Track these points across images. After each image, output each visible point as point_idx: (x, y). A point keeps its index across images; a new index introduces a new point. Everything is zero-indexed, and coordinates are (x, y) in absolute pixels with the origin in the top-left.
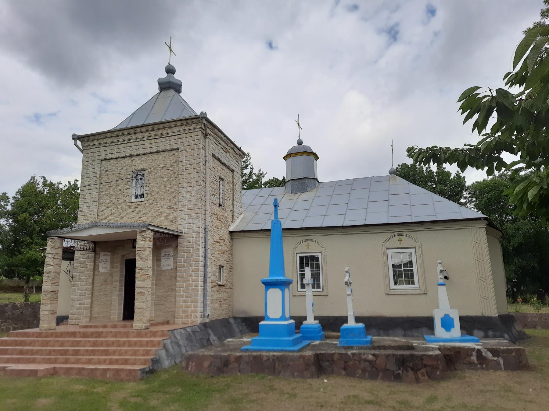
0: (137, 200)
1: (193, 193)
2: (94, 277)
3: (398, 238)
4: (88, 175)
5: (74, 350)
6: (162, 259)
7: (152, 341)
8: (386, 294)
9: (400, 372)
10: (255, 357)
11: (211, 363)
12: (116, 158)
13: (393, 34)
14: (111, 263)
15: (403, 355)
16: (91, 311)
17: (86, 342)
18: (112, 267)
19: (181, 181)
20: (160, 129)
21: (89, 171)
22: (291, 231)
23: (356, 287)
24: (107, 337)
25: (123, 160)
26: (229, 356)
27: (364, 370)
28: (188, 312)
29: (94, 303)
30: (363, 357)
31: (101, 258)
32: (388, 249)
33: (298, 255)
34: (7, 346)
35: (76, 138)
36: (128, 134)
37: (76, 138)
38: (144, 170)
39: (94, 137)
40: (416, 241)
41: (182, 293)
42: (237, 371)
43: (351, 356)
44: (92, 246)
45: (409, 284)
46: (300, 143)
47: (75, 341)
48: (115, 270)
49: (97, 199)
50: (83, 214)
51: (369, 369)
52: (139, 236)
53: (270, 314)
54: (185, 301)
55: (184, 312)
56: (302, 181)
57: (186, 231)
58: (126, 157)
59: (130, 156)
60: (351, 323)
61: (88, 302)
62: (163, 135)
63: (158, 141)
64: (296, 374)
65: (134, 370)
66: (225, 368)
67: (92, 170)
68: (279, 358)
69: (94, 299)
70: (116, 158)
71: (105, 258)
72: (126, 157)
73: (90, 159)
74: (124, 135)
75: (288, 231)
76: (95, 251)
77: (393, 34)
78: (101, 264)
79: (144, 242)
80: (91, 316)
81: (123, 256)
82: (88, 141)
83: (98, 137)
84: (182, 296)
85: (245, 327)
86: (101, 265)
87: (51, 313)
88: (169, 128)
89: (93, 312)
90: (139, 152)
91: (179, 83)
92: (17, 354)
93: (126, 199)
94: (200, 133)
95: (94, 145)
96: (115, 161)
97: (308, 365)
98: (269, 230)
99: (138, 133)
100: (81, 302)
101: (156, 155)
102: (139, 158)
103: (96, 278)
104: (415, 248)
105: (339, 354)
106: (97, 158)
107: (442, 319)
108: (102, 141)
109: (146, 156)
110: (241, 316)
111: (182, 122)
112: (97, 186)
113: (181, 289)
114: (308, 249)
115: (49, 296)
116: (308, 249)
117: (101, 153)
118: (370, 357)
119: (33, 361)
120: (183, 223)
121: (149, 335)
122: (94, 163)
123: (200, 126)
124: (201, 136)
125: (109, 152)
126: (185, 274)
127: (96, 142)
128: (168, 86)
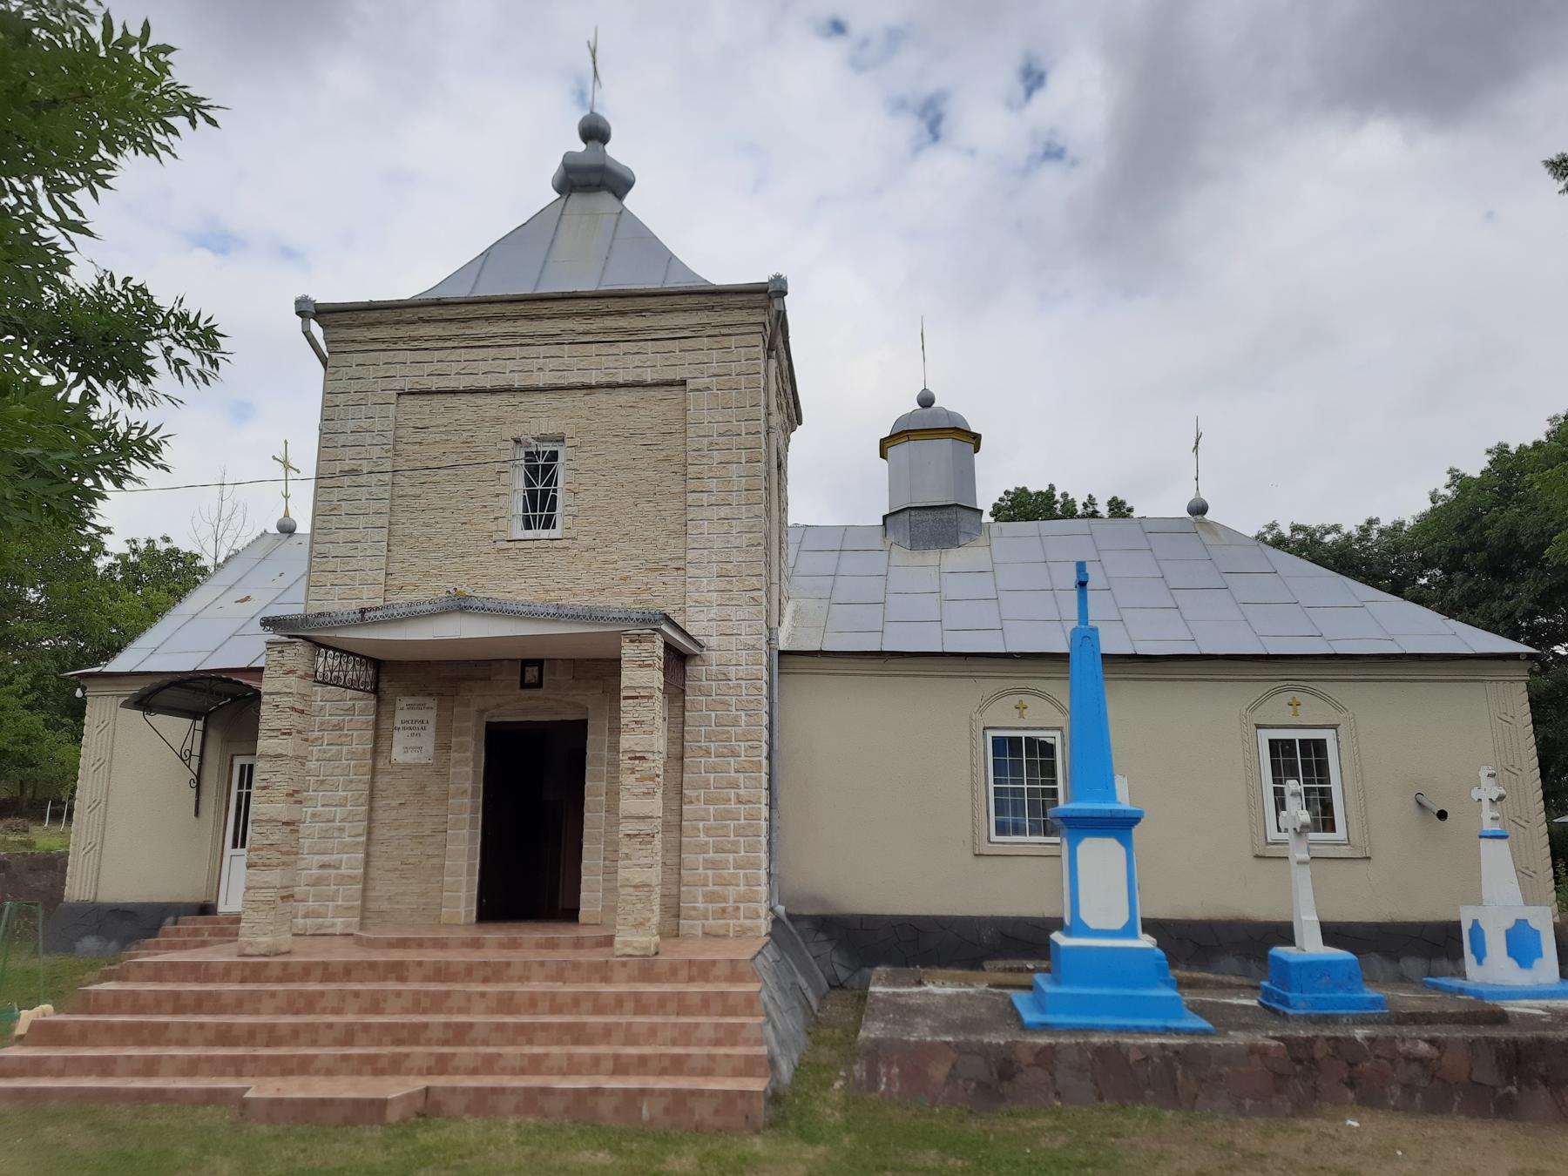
0: (530, 534)
1: (737, 526)
3: (1287, 697)
4: (351, 437)
5: (447, 1025)
8: (1257, 857)
9: (1514, 1090)
10: (1100, 1051)
11: (954, 1066)
12: (454, 392)
13: (932, 120)
14: (438, 730)
15: (1515, 1042)
16: (365, 890)
17: (342, 995)
18: (443, 747)
19: (692, 484)
20: (622, 313)
21: (351, 425)
22: (970, 661)
23: (1182, 827)
24: (528, 979)
25: (480, 400)
26: (1010, 1046)
27: (1409, 1088)
28: (725, 900)
30: (1402, 1048)
31: (400, 716)
32: (1258, 727)
33: (990, 734)
34: (101, 1012)
35: (308, 310)
36: (595, 314)
37: (308, 310)
38: (560, 439)
39: (376, 315)
40: (1339, 708)
41: (703, 838)
42: (1051, 1095)
43: (1366, 1044)
44: (367, 674)
45: (1325, 830)
46: (926, 401)
47: (427, 993)
48: (454, 755)
49: (384, 520)
50: (331, 567)
51: (1424, 1083)
52: (628, 650)
53: (1091, 916)
54: (713, 865)
55: (711, 897)
56: (945, 515)
57: (713, 642)
58: (493, 391)
60: (1310, 945)
61: (351, 862)
64: (1248, 1103)
65: (742, 1093)
66: (1006, 1084)
67: (365, 424)
68: (1177, 1051)
69: (375, 849)
70: (454, 392)
71: (416, 715)
72: (493, 391)
73: (356, 385)
74: (487, 319)
75: (961, 661)
76: (376, 691)
77: (932, 120)
78: (397, 736)
79: (646, 672)
80: (364, 909)
81: (481, 712)
82: (349, 327)
84: (703, 848)
85: (828, 948)
86: (400, 738)
87: (283, 898)
88: (655, 312)
89: (370, 894)
90: (542, 380)
92: (210, 1043)
94: (758, 339)
95: (374, 340)
96: (449, 401)
97: (1279, 1076)
98: (1063, 658)
99: (540, 318)
100: (326, 859)
101: (601, 397)
102: (542, 398)
103: (382, 781)
104: (1335, 727)
105: (1328, 1039)
106: (382, 384)
107: (1507, 932)
108: (404, 331)
109: (568, 399)
110: (806, 912)
111: (702, 299)
112: (387, 478)
113: (701, 825)
114: (1021, 716)
116: (1021, 716)
117: (397, 370)
118: (1423, 1047)
119: (303, 1067)
120: (702, 616)
121: (683, 974)
122: (371, 399)
123: (760, 319)
124: (760, 351)
125: (428, 368)
128: (595, 178)
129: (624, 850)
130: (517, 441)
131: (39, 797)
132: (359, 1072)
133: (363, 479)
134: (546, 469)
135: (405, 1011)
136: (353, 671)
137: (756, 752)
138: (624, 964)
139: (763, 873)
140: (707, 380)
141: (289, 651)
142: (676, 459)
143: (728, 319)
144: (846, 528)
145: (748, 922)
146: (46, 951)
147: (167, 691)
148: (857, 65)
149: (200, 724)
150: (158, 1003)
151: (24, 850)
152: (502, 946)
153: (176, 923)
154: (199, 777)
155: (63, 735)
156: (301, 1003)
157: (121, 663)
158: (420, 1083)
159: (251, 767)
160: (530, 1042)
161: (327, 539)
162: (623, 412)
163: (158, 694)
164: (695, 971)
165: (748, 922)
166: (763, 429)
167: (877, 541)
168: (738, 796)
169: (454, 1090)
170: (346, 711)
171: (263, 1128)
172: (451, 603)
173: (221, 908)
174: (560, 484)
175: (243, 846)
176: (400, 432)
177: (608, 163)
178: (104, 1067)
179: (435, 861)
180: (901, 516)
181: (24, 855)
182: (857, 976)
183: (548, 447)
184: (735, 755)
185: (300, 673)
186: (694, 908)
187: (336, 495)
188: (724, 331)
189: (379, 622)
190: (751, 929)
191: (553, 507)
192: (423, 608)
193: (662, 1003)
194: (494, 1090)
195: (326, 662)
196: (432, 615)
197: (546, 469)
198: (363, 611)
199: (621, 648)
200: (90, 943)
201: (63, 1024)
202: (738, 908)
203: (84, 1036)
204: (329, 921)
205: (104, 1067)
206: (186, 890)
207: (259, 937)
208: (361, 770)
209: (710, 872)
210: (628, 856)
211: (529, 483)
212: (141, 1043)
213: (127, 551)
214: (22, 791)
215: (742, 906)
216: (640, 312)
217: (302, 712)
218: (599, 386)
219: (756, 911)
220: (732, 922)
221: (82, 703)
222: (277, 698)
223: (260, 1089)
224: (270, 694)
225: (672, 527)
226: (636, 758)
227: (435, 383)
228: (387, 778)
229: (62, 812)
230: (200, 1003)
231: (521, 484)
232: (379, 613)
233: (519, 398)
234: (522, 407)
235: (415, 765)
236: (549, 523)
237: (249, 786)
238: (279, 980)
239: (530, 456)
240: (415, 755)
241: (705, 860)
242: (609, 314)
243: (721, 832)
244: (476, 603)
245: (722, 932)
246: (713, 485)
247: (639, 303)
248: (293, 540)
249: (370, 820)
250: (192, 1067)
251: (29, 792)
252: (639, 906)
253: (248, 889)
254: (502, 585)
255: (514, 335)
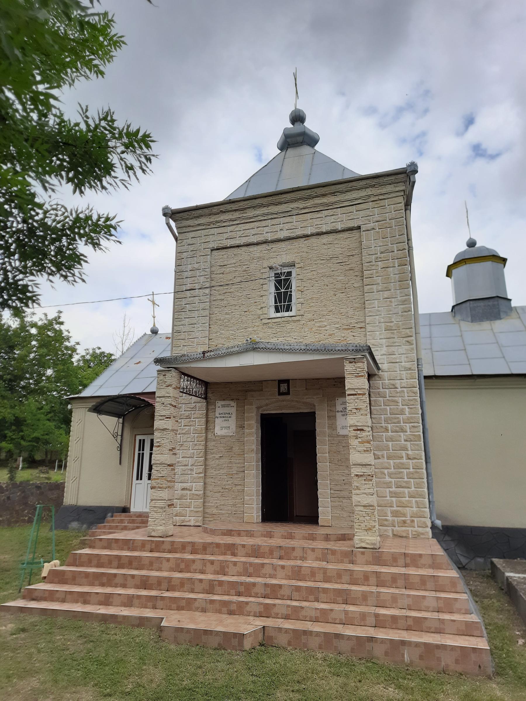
2: (206, 442)
6: (339, 415)
7: (406, 576)
16: (204, 502)
20: (324, 195)
21: (190, 267)
24: (306, 559)
28: (404, 515)
29: (210, 488)
31: (218, 411)
36: (262, 206)
39: (200, 212)
41: (388, 479)
46: (471, 244)
48: (246, 431)
49: (207, 313)
52: (348, 367)
55: (395, 514)
56: (491, 303)
58: (257, 244)
59: (266, 242)
62: (327, 205)
63: (319, 215)
67: (196, 266)
70: (238, 246)
71: (226, 410)
72: (257, 244)
73: (191, 248)
76: (206, 398)
80: (204, 512)
81: (258, 408)
82: (187, 219)
83: (206, 211)
87: (169, 505)
88: (342, 192)
89: (207, 504)
90: (282, 235)
91: (316, 137)
93: (260, 312)
94: (401, 199)
95: (199, 225)
96: (236, 251)
99: (280, 203)
100: (185, 485)
101: (313, 240)
102: (283, 245)
103: (211, 444)
108: (213, 219)
111: (368, 181)
112: (207, 291)
113: (386, 471)
115: (163, 473)
125: (226, 236)
126: (390, 444)
127: (202, 221)
128: (300, 139)
129: (355, 484)
130: (271, 268)
131: (53, 459)
132: (220, 612)
133: (197, 292)
134: (286, 280)
135: (239, 574)
136: (194, 386)
137: (416, 429)
138: (363, 553)
139: (427, 500)
140: (372, 224)
141: (168, 375)
142: (357, 269)
143: (384, 191)
144: (430, 314)
145: (420, 530)
146: (56, 528)
147: (107, 404)
148: (382, 126)
149: (121, 420)
150: (110, 562)
151: (46, 481)
152: (284, 537)
153: (112, 516)
154: (121, 445)
155: (62, 431)
156: (183, 566)
157: (87, 393)
158: (260, 623)
159: (144, 440)
160: (317, 600)
161: (180, 323)
162: (326, 247)
163: (103, 406)
164: (408, 560)
165: (420, 530)
166: (407, 247)
167: (450, 319)
168: (408, 455)
169: (280, 629)
170: (194, 405)
171: (172, 647)
172: (248, 346)
173: (132, 510)
174: (294, 287)
175: (141, 479)
176: (213, 269)
177: (307, 131)
178: (84, 598)
179: (239, 487)
180: (464, 305)
181: (47, 483)
182: (473, 561)
183: (286, 270)
184: (403, 431)
185: (173, 386)
186: (386, 520)
187: (184, 301)
188: (381, 197)
189: (212, 358)
190: (423, 534)
191: (290, 300)
192: (234, 349)
193: (394, 580)
194: (305, 632)
195: (185, 383)
196: (239, 353)
197: (286, 280)
198: (204, 353)
199: (344, 366)
200: (75, 525)
201: (64, 572)
202: (413, 521)
203: (74, 579)
204: (187, 518)
205: (84, 598)
206: (117, 502)
207: (158, 526)
208: (201, 439)
209: (394, 499)
210: (358, 488)
211: (277, 288)
212: (103, 585)
213: (84, 354)
214: (46, 456)
215: (415, 520)
216: (333, 194)
217: (175, 406)
218: (312, 235)
219: (425, 523)
220: (410, 529)
221: (71, 412)
222: (163, 399)
223: (172, 619)
224: (160, 397)
225: (356, 305)
226: (358, 430)
227: (230, 243)
228: (213, 443)
229: (62, 466)
230: (131, 563)
231: (273, 289)
232: (212, 353)
233: (271, 246)
234: (273, 250)
235: (227, 436)
236: (288, 308)
237: (143, 450)
238: (170, 552)
239: (277, 275)
240: (226, 431)
241: (390, 492)
242: (317, 197)
243: (398, 476)
244: (262, 346)
245: (404, 535)
246: (379, 280)
247: (333, 188)
248: (157, 336)
249: (206, 465)
250: (129, 602)
251: (49, 457)
252: (368, 518)
253: (152, 500)
254: (266, 341)
255: (268, 214)
